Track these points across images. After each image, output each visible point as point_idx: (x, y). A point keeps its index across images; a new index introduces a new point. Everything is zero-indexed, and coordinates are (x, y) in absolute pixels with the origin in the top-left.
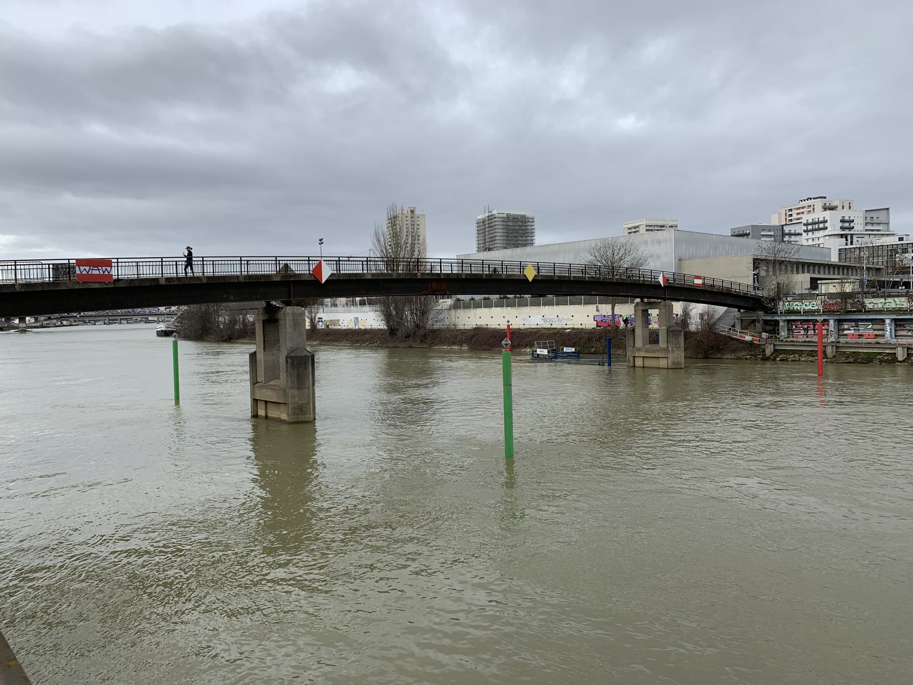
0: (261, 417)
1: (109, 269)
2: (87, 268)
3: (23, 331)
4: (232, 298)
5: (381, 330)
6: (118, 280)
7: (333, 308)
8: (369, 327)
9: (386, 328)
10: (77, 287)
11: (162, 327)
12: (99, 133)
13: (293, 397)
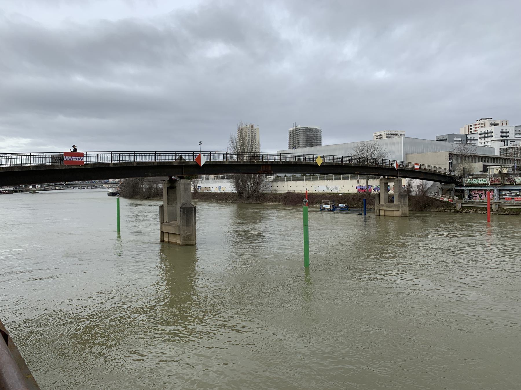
1: (82, 158)
2: (70, 157)
3: (34, 192)
4: (150, 174)
6: (87, 164)
8: (227, 192)
9: (236, 192)
10: (64, 168)
11: (111, 190)
12: (80, 81)
13: (184, 231)
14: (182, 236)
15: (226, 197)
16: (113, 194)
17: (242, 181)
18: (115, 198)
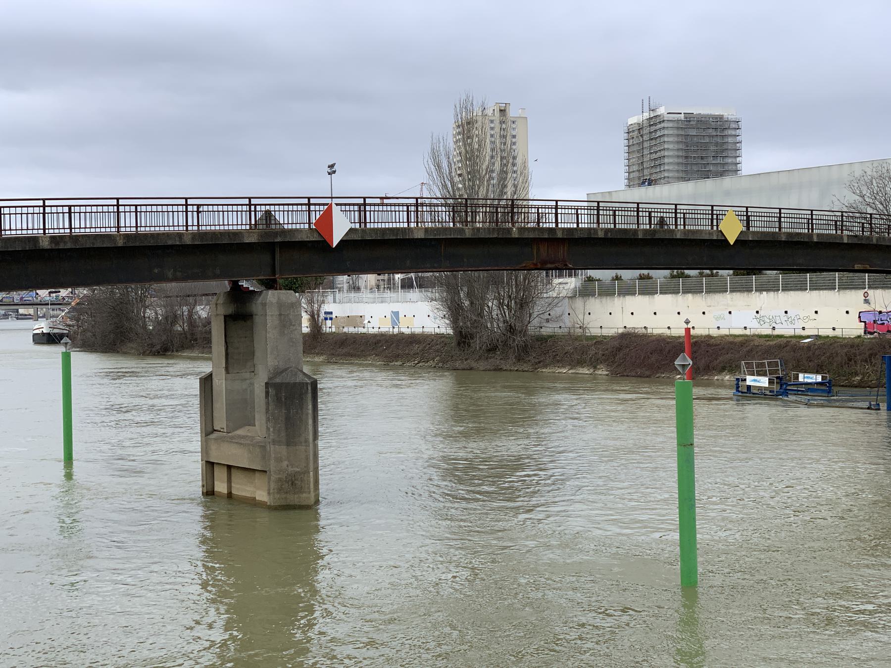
0: (220, 495)
4: (170, 274)
5: (442, 336)
7: (352, 294)
8: (418, 331)
11: (43, 326)
13: (279, 460)
14: (274, 477)
15: (416, 348)
16: (49, 339)
17: (469, 295)
18: (57, 351)
